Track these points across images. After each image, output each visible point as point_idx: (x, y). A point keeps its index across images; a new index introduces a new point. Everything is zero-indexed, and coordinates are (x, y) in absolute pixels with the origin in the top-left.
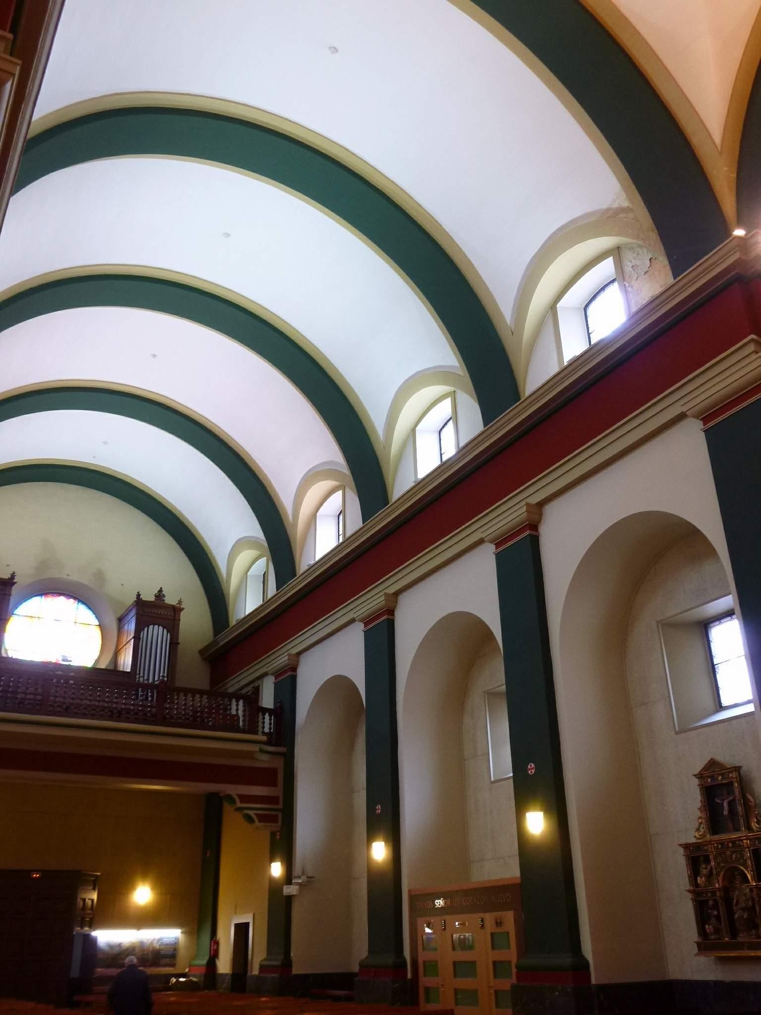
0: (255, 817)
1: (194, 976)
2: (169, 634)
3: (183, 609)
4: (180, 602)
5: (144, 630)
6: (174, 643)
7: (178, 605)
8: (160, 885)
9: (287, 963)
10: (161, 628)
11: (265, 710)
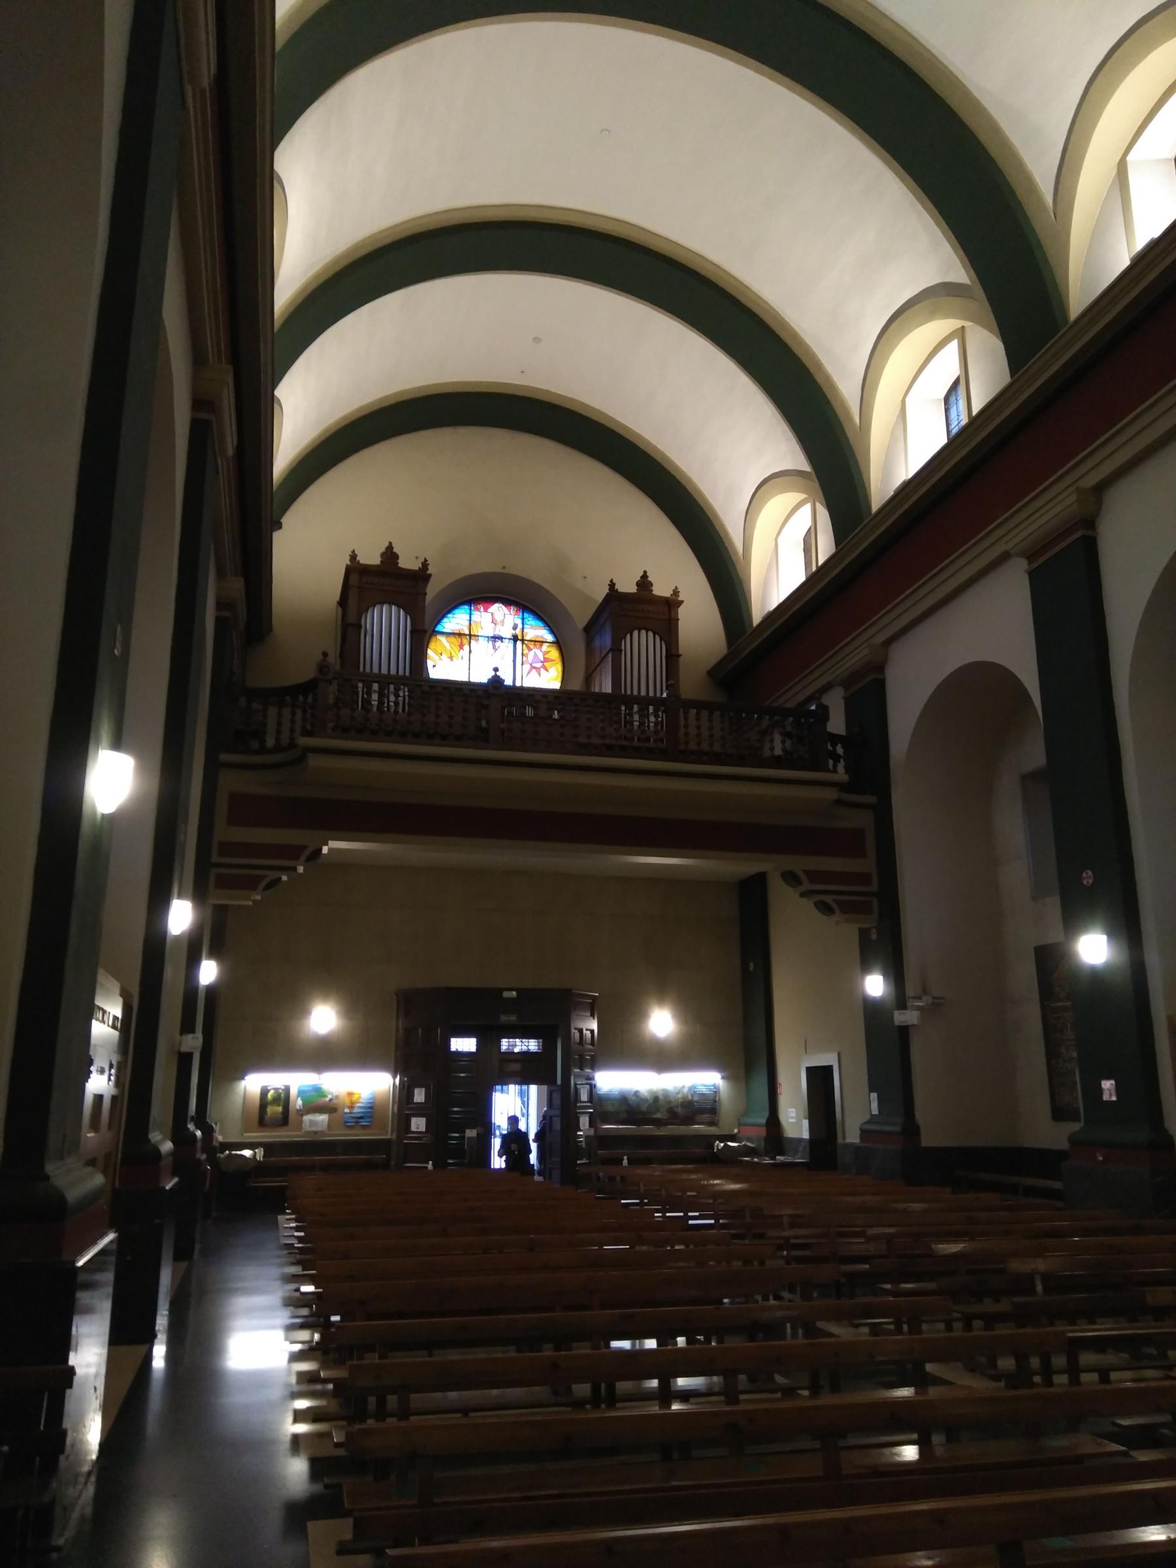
0: (835, 906)
1: (749, 1140)
2: (663, 642)
3: (683, 601)
4: (676, 592)
5: (625, 638)
6: (672, 657)
7: (674, 597)
8: (351, 1008)
9: (911, 1129)
10: (651, 634)
11: (835, 739)
